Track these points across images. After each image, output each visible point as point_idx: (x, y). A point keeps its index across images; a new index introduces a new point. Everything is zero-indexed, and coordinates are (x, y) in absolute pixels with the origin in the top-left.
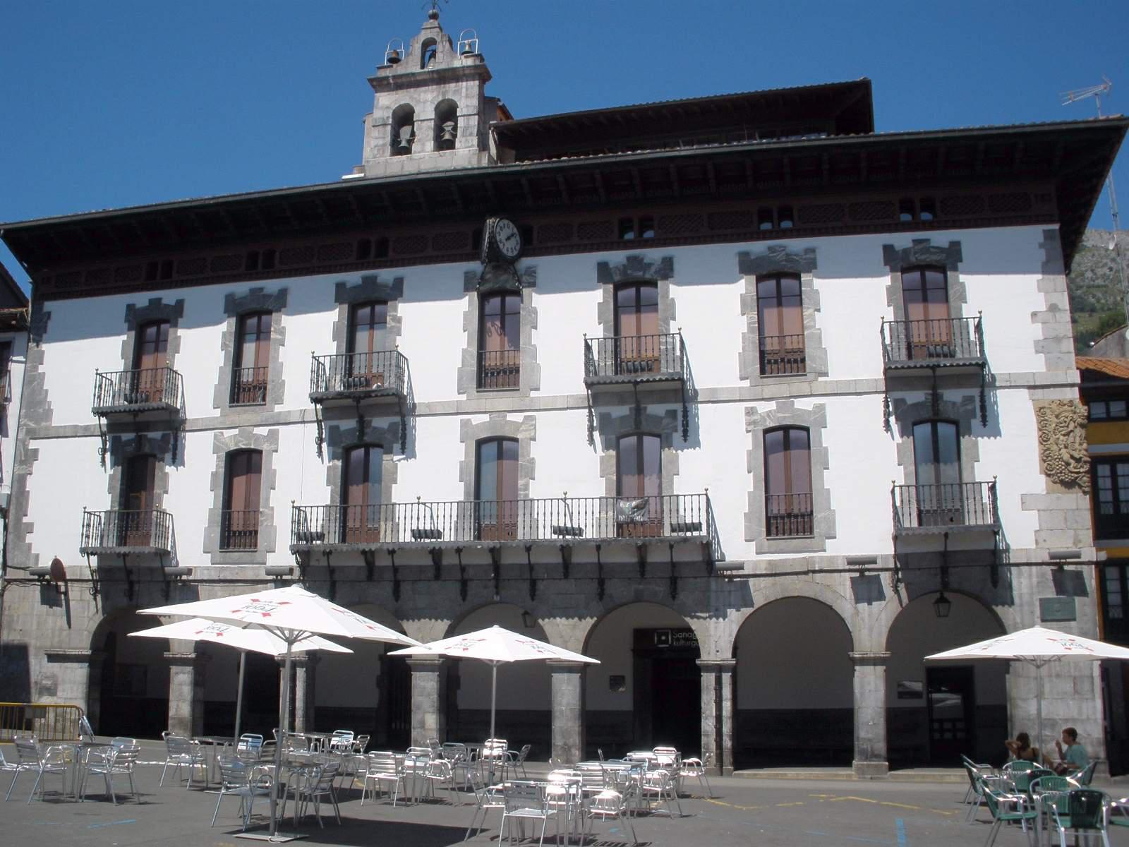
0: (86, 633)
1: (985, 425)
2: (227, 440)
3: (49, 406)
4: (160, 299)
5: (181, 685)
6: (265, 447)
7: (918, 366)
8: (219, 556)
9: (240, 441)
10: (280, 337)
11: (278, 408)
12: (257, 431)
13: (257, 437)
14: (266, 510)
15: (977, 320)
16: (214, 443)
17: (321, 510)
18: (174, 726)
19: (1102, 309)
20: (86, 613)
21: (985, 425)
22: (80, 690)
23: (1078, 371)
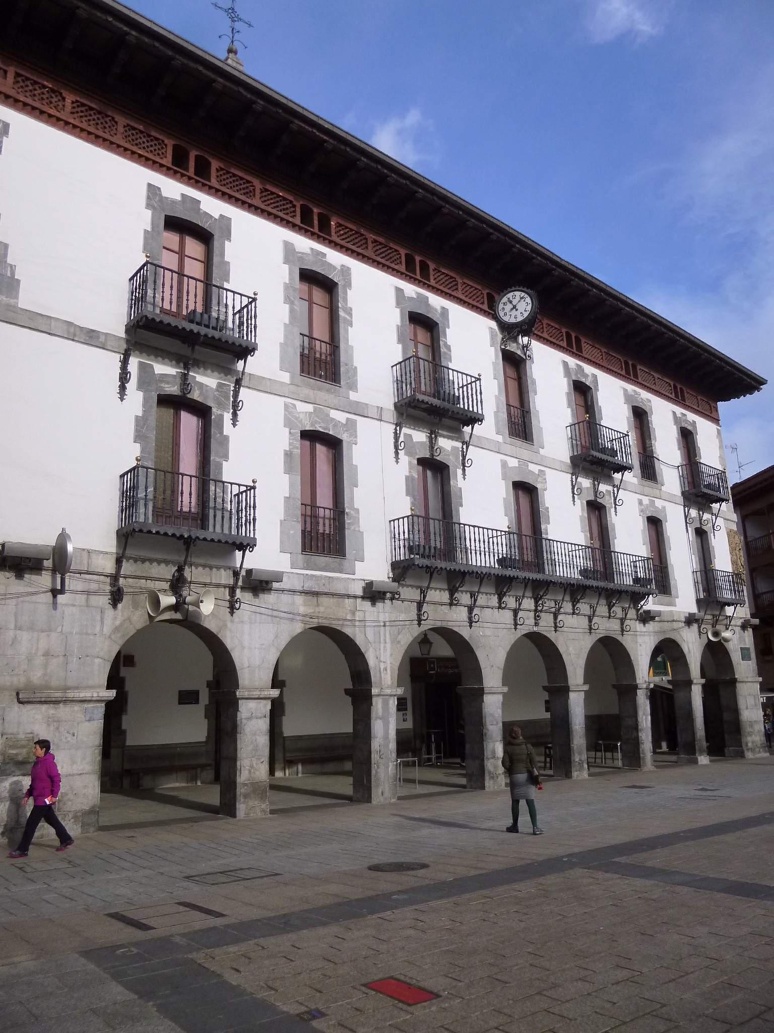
0: (97, 661)
1: (122, 399)
2: (302, 416)
3: (13, 273)
4: (199, 202)
5: (255, 734)
6: (344, 437)
7: (162, 532)
8: (300, 557)
9: (316, 422)
10: (348, 317)
11: (353, 396)
12: (334, 414)
13: (336, 424)
14: (352, 512)
15: (245, 301)
16: (285, 415)
17: (406, 519)
18: (246, 796)
19: (107, 116)
20: (98, 629)
21: (122, 399)
22: (88, 759)
23: (615, 691)
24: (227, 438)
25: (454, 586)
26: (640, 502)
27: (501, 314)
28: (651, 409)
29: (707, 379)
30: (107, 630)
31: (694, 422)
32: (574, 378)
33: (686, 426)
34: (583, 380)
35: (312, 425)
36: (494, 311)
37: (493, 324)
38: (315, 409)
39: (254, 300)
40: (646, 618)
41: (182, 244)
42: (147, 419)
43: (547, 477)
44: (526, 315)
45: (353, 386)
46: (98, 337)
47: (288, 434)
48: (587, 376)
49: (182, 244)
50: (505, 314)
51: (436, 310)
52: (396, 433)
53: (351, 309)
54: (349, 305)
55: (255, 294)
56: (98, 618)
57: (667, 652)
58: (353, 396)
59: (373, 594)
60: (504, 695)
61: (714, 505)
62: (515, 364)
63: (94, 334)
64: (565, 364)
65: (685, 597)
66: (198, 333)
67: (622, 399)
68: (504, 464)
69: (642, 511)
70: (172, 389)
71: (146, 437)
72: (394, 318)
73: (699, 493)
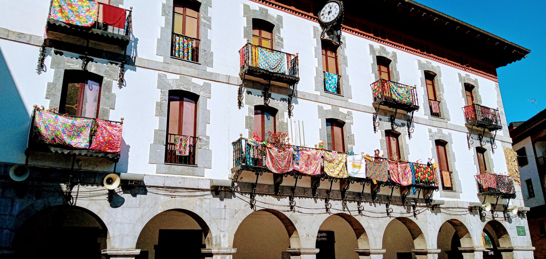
2: (170, 82)
13: (195, 86)
14: (204, 138)
21: (240, 108)
24: (114, 96)
25: (404, 194)
26: (430, 131)
27: (322, 17)
28: (440, 72)
29: (484, 53)
30: (15, 213)
31: (476, 80)
32: (378, 55)
33: (469, 82)
34: (385, 56)
35: (178, 86)
36: (318, 16)
37: (318, 25)
38: (180, 77)
39: (297, 57)
40: (435, 207)
41: (260, 33)
42: (56, 85)
43: (353, 116)
44: (336, 16)
45: (211, 64)
46: (25, 37)
47: (160, 93)
48: (388, 53)
49: (260, 33)
50: (324, 18)
51: (273, 17)
52: (374, 118)
53: (210, 18)
54: (209, 15)
55: (131, 8)
56: (10, 204)
57: (454, 232)
58: (209, 69)
59: (217, 191)
60: (439, 254)
61: (492, 132)
62: (330, 46)
63: (22, 36)
64: (371, 47)
65: (469, 194)
66: (102, 35)
67: (458, 79)
68: (320, 108)
69: (431, 136)
70: (75, 66)
71: (54, 95)
72: (371, 60)
73: (481, 124)
